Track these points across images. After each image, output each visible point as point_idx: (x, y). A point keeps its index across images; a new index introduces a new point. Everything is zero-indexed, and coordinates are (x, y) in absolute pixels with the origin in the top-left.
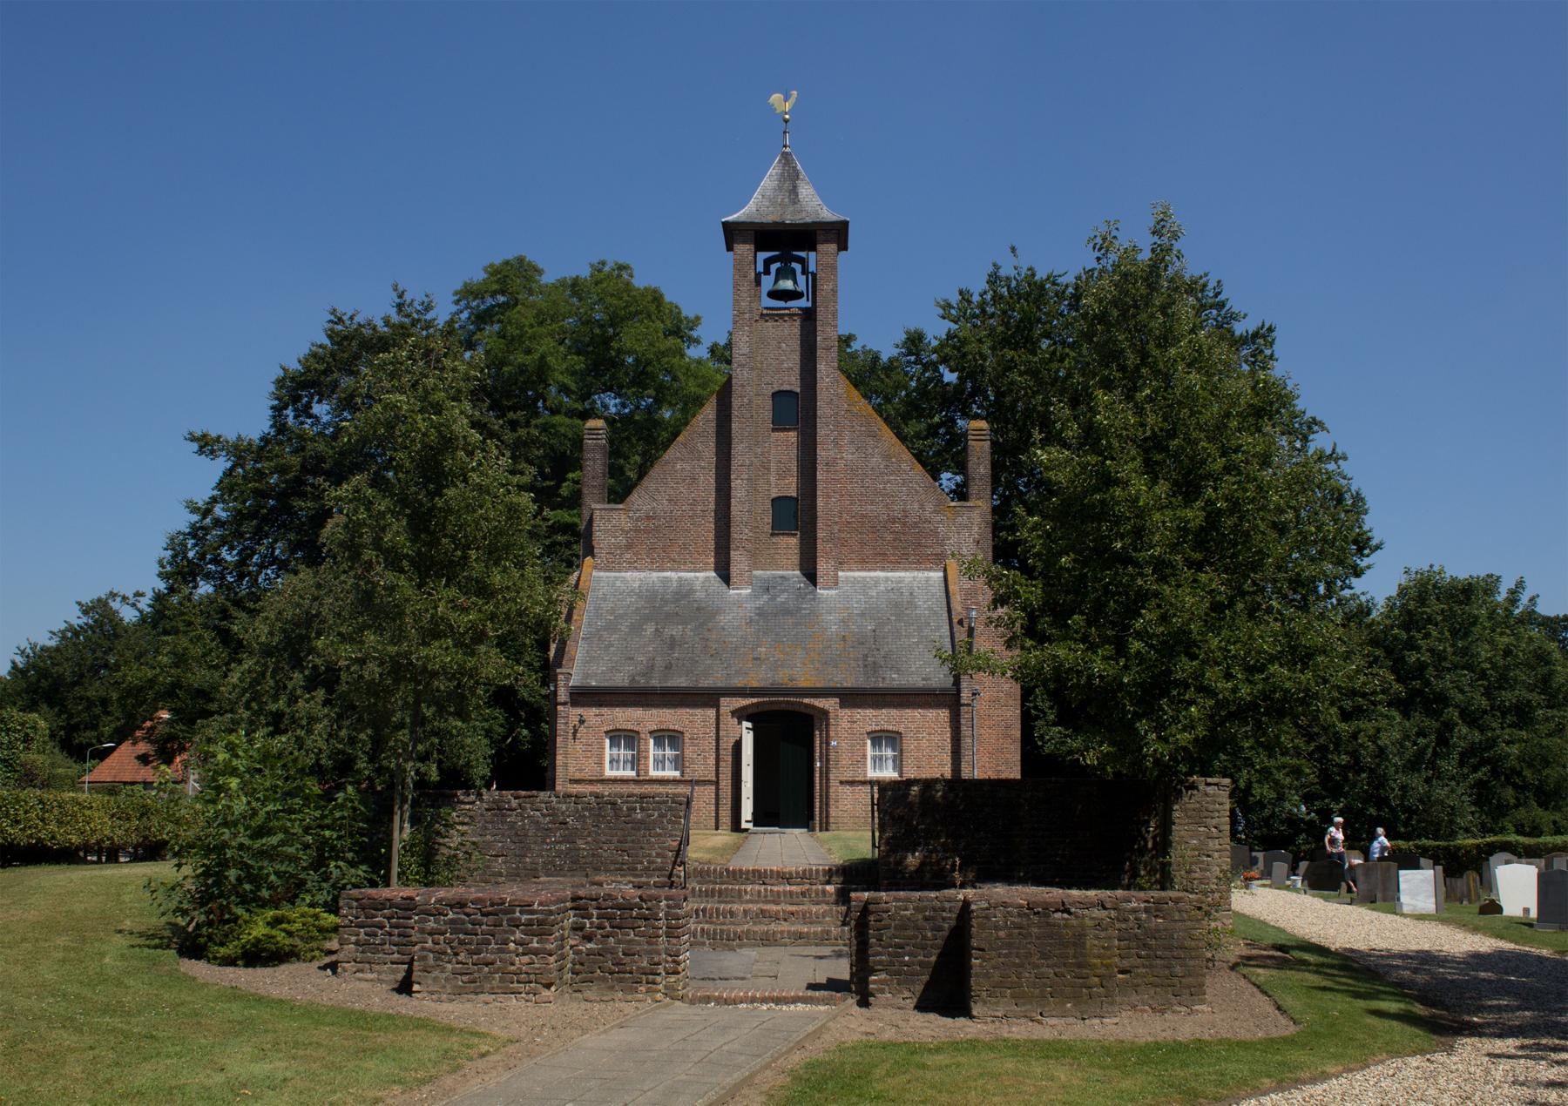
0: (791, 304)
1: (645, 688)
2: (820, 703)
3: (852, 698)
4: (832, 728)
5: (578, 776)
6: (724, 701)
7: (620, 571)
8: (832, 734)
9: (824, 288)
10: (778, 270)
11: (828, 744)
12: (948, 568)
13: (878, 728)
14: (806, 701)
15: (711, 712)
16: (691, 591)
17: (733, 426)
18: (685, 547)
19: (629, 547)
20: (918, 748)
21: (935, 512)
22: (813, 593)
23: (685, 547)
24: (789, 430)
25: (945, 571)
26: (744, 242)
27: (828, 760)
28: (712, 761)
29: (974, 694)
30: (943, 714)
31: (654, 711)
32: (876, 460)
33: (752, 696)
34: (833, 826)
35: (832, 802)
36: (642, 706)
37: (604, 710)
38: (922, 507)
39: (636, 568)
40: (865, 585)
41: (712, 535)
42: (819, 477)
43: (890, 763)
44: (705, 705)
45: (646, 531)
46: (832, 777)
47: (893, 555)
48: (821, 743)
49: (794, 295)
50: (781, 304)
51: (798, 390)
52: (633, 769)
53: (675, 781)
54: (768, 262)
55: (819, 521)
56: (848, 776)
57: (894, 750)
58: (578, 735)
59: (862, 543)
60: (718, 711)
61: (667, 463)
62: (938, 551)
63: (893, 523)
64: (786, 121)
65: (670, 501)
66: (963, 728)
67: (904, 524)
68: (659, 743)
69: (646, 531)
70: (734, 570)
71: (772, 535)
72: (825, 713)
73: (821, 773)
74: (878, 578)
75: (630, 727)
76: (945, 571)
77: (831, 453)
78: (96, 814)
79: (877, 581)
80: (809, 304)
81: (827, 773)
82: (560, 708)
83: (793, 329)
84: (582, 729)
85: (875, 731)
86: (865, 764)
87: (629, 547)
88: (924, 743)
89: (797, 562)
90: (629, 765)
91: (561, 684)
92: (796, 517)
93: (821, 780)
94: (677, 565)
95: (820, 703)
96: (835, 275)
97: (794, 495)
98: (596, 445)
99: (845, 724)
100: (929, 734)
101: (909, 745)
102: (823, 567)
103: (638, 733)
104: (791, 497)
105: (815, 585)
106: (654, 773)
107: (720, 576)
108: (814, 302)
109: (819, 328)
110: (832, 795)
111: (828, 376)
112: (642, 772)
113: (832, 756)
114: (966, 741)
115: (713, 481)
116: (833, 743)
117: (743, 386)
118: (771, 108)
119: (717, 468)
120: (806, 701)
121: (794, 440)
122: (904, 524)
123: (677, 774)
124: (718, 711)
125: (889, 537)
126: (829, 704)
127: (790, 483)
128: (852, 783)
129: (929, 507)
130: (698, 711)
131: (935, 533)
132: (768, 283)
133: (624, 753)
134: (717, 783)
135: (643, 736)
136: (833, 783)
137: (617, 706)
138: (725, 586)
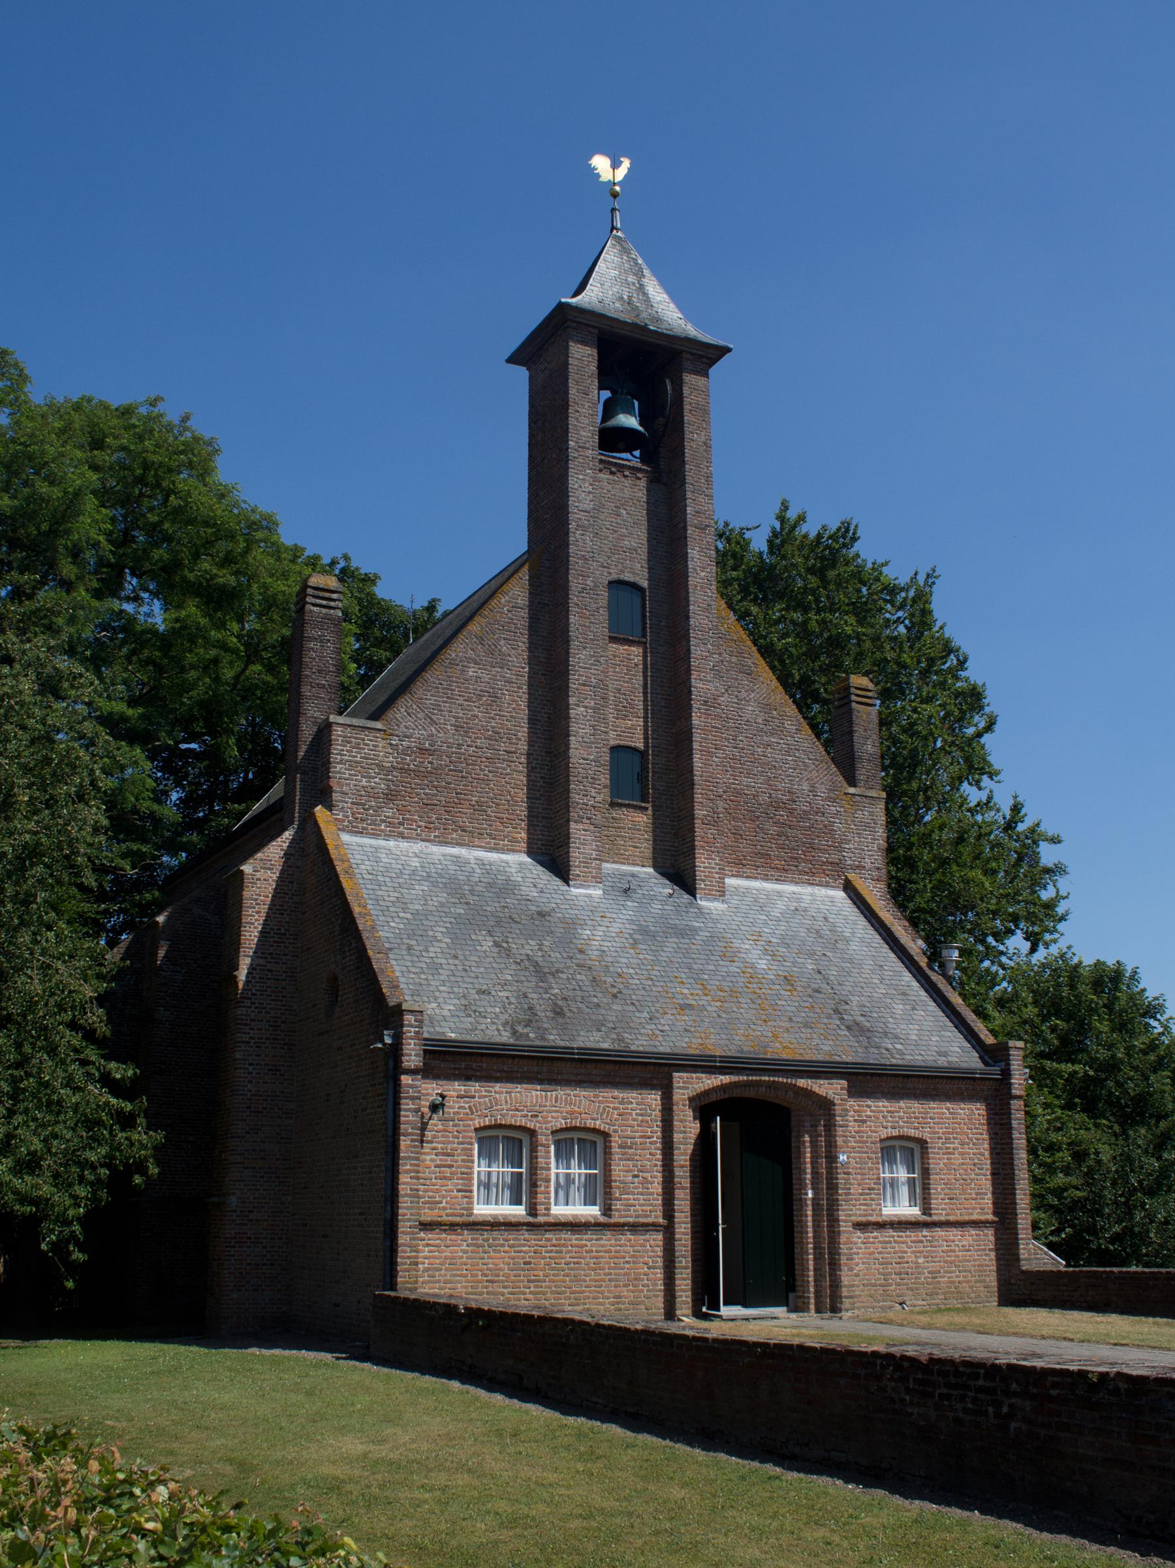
1: (539, 1049)
4: (839, 1131)
6: (679, 1078)
7: (375, 836)
8: (840, 1141)
11: (832, 1158)
13: (895, 1133)
14: (802, 1082)
15: (654, 1098)
17: (572, 619)
18: (479, 807)
19: (390, 796)
21: (829, 799)
23: (479, 807)
24: (630, 643)
26: (584, 343)
28: (657, 1187)
31: (561, 1093)
32: (751, 710)
33: (723, 1070)
34: (846, 1303)
35: (843, 1260)
36: (541, 1082)
37: (475, 1087)
38: (813, 789)
39: (402, 836)
40: (761, 904)
41: (522, 795)
43: (904, 1191)
44: (645, 1084)
45: (417, 773)
47: (778, 858)
51: (645, 584)
52: (589, 1201)
55: (698, 790)
57: (911, 1169)
58: (429, 1135)
61: (453, 664)
62: (834, 858)
63: (777, 808)
64: (615, 195)
65: (457, 727)
67: (791, 812)
68: (563, 1154)
69: (417, 773)
71: (613, 805)
72: (826, 1106)
75: (519, 1121)
77: (711, 686)
82: (406, 1079)
84: (435, 1123)
87: (390, 796)
88: (957, 1159)
89: (648, 853)
90: (507, 1193)
91: (409, 1031)
93: (817, 1227)
94: (469, 837)
96: (708, 423)
97: (640, 745)
98: (326, 617)
100: (962, 1144)
101: (937, 1162)
102: (705, 864)
105: (691, 891)
106: (560, 1211)
110: (844, 1248)
111: (703, 569)
112: (541, 1209)
115: (523, 706)
116: (842, 1158)
117: (584, 558)
118: (593, 174)
119: (530, 686)
120: (802, 1082)
121: (638, 659)
122: (791, 812)
123: (592, 1212)
125: (773, 830)
126: (832, 1089)
127: (633, 727)
129: (822, 791)
130: (632, 1095)
131: (829, 830)
133: (502, 1170)
134: (669, 1230)
135: (542, 1139)
136: (845, 1227)
137: (498, 1080)
138: (557, 882)
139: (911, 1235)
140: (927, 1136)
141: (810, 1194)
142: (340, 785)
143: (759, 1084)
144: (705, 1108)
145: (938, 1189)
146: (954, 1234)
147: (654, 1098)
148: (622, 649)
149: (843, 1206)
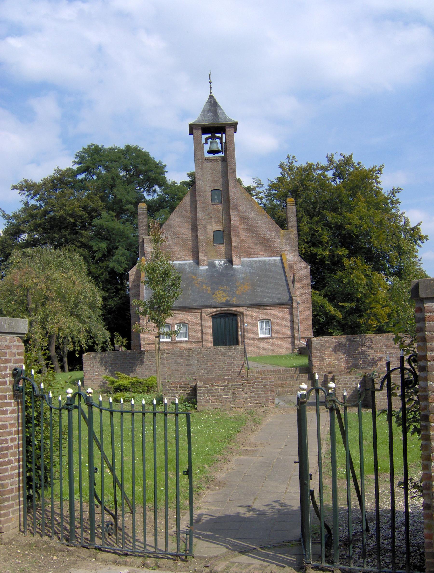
0: (216, 155)
2: (240, 309)
3: (251, 306)
4: (245, 319)
5: (148, 342)
6: (203, 310)
8: (245, 321)
9: (229, 148)
10: (211, 143)
11: (244, 325)
12: (283, 256)
14: (235, 309)
15: (199, 315)
16: (185, 269)
20: (278, 325)
22: (232, 267)
25: (281, 256)
27: (244, 332)
28: (200, 333)
29: (298, 304)
30: (285, 312)
33: (214, 307)
42: (232, 223)
46: (246, 337)
47: (261, 251)
48: (241, 325)
49: (217, 152)
50: (212, 155)
51: (221, 189)
53: (186, 342)
54: (207, 139)
56: (252, 337)
59: (249, 247)
60: (201, 315)
61: (172, 219)
66: (294, 317)
70: (201, 261)
73: (241, 337)
74: (256, 261)
76: (281, 256)
78: (332, 282)
79: (256, 262)
80: (223, 155)
81: (244, 336)
83: (219, 165)
85: (261, 320)
86: (258, 332)
92: (223, 238)
93: (241, 339)
95: (240, 309)
97: (222, 230)
98: (143, 213)
99: (249, 317)
100: (282, 320)
101: (274, 324)
103: (170, 324)
104: (220, 231)
107: (195, 262)
108: (226, 154)
109: (228, 165)
111: (233, 183)
113: (245, 330)
114: (296, 322)
120: (235, 309)
122: (265, 239)
124: (201, 315)
128: (253, 339)
132: (207, 147)
135: (173, 325)
139: (266, 341)
140: (271, 319)
141: (240, 333)
142: (147, 252)
143: (224, 310)
144: (214, 317)
145: (274, 330)
146: (279, 340)
147: (199, 315)
148: (215, 206)
149: (246, 335)
